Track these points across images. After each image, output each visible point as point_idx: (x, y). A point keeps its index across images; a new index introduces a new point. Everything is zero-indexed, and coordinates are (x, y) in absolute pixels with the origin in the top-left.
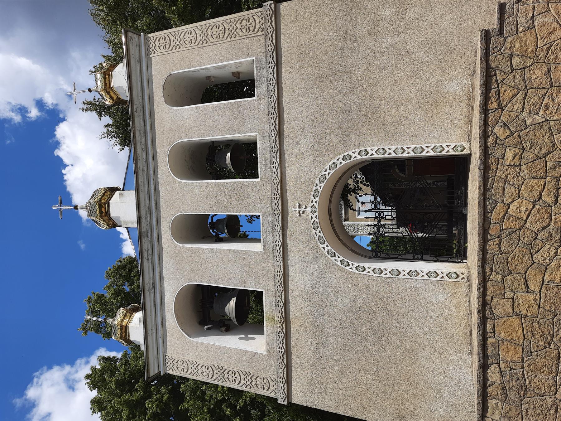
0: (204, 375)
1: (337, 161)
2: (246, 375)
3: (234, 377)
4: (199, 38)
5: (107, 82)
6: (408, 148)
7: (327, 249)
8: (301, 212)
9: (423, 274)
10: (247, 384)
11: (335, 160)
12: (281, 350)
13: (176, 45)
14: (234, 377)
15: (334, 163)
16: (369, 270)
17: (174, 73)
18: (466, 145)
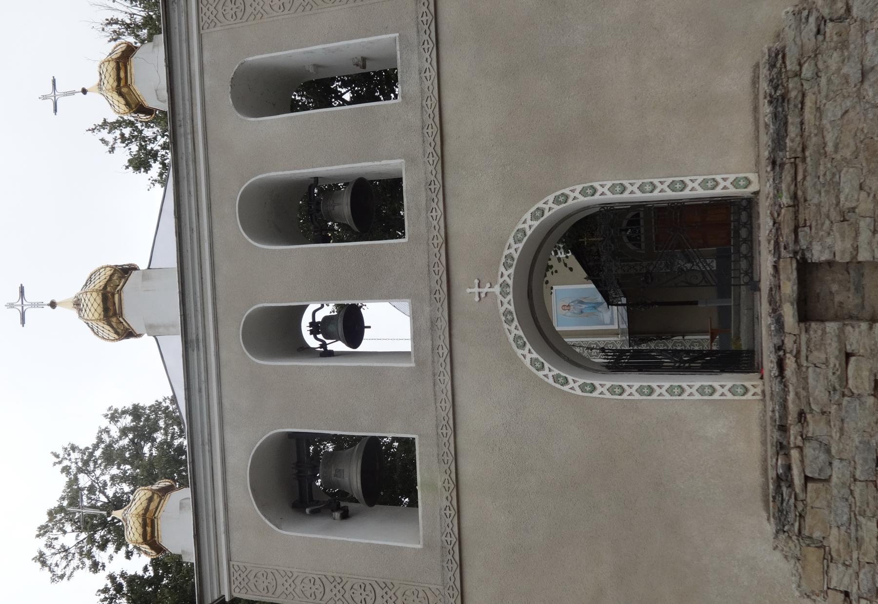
0: (261, 589)
1: (544, 206)
2: (239, 572)
3: (314, 588)
4: (249, 10)
5: (122, 75)
6: (662, 183)
7: (529, 356)
8: (483, 295)
9: (691, 390)
10: (287, 593)
11: (540, 204)
12: (449, 539)
13: (255, 13)
14: (364, 594)
15: (538, 209)
16: (691, 390)
17: (250, 59)
18: (753, 177)
